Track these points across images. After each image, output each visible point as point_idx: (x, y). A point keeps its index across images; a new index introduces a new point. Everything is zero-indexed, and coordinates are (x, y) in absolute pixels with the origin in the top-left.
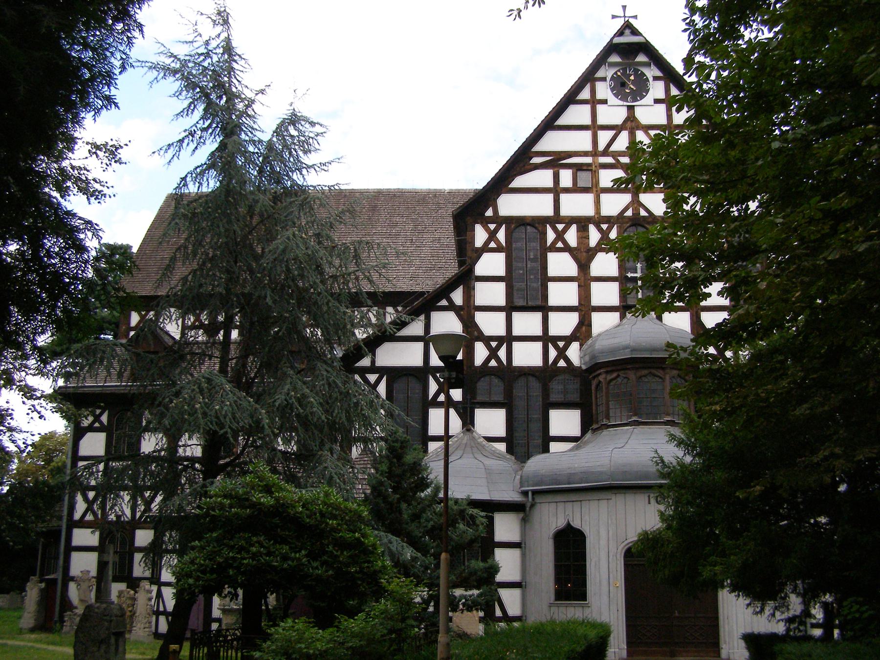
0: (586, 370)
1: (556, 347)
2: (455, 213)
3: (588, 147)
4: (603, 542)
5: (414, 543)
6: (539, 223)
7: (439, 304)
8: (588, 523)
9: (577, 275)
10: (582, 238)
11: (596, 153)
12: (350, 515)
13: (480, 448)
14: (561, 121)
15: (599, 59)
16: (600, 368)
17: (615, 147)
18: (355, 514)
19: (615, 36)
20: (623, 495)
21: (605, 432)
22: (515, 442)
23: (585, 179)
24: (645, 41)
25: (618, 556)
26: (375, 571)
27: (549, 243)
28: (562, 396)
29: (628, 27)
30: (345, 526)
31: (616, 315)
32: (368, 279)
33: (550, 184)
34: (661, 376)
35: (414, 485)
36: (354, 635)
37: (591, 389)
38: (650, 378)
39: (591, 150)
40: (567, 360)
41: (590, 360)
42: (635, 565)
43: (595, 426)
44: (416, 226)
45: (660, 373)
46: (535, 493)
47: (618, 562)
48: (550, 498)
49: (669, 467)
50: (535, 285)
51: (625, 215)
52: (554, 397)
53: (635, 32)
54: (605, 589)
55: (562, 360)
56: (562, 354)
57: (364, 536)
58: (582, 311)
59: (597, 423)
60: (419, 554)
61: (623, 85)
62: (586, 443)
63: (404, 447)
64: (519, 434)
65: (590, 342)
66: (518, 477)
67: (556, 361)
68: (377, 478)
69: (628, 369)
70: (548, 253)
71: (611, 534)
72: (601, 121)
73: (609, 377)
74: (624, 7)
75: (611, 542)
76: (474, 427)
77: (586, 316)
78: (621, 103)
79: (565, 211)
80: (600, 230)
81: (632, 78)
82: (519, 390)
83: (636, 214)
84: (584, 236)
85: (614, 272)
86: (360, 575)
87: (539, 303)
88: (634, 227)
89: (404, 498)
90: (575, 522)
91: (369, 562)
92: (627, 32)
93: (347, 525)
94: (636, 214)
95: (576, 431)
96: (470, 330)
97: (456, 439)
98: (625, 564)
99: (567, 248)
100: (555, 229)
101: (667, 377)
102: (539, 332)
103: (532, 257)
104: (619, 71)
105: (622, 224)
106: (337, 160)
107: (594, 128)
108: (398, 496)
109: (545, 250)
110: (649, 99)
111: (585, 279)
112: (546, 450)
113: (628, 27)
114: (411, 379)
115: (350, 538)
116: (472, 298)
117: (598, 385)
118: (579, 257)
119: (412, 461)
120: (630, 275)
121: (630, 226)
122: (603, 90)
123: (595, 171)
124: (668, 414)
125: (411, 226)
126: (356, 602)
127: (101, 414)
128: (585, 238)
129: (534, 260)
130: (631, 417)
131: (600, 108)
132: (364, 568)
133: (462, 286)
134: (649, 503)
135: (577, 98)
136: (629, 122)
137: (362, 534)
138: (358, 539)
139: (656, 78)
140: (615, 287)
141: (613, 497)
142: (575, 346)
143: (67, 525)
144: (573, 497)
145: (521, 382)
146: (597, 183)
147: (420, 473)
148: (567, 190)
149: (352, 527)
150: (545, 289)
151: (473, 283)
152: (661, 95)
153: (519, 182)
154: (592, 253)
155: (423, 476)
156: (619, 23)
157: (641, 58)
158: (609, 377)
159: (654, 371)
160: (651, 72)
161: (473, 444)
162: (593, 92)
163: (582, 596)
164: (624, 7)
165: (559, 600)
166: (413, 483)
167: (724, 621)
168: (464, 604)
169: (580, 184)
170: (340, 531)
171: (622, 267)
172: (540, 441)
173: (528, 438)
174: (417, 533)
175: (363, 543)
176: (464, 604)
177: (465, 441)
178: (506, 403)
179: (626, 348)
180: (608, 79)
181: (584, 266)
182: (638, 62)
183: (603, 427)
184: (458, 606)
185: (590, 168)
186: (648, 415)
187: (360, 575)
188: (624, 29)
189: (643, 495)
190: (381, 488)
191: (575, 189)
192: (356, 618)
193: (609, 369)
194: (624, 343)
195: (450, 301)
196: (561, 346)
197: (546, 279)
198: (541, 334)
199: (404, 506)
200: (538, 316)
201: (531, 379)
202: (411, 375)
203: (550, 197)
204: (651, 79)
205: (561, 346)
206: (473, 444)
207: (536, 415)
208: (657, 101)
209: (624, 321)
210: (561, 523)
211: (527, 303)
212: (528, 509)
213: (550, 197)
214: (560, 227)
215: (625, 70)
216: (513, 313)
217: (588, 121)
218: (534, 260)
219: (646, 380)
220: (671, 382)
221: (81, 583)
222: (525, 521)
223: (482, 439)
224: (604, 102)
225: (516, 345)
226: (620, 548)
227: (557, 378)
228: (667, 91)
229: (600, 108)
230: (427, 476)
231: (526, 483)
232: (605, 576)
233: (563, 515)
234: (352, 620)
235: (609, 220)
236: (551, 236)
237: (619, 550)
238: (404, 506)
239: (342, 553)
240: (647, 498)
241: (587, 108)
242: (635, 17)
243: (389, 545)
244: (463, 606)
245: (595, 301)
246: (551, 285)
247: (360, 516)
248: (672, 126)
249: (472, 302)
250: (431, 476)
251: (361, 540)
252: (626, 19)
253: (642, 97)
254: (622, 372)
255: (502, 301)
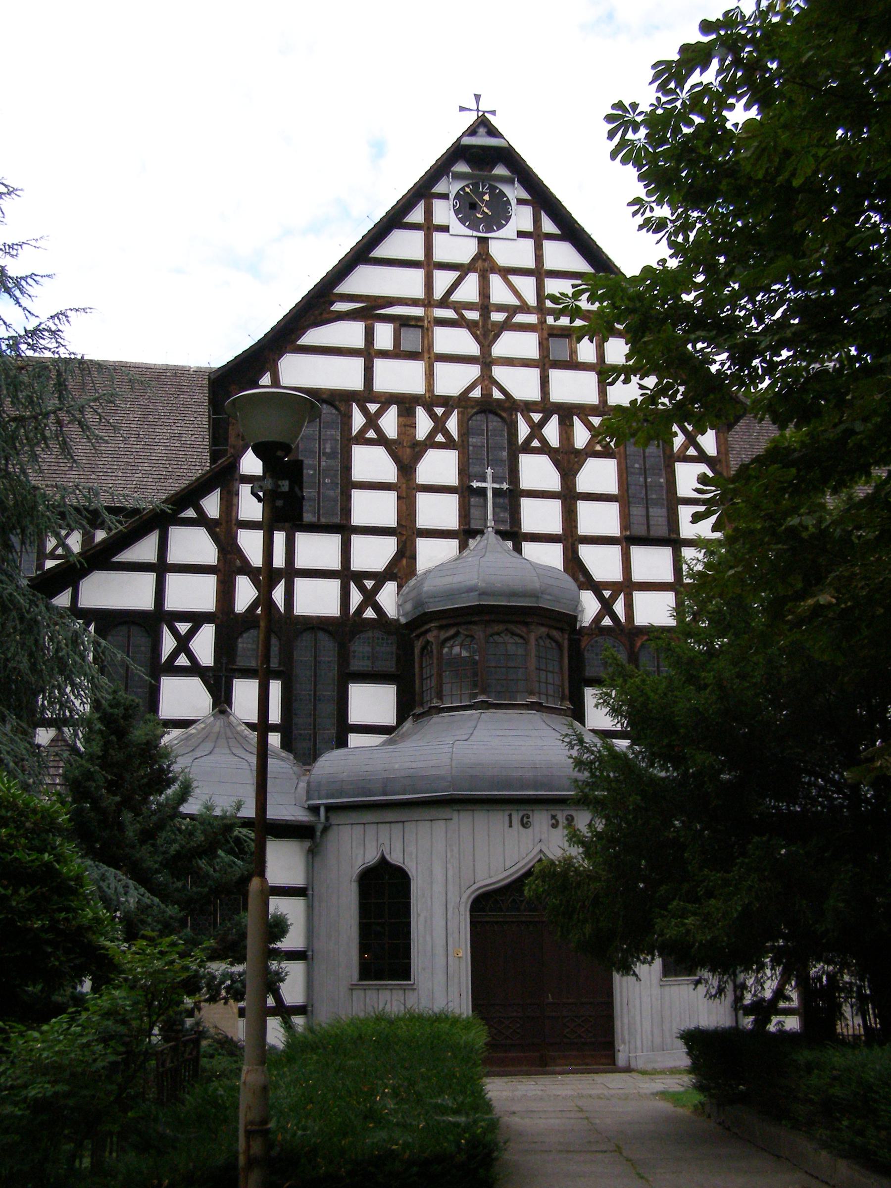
0: (407, 624)
1: (362, 588)
2: (212, 377)
3: (419, 293)
4: (438, 888)
5: (142, 878)
6: (340, 401)
7: (182, 515)
8: (414, 856)
9: (396, 481)
10: (405, 426)
11: (429, 302)
12: (33, 818)
13: (239, 738)
14: (380, 252)
15: (440, 166)
16: (431, 621)
17: (458, 296)
18: (43, 817)
19: (463, 134)
20: (470, 813)
21: (436, 719)
22: (295, 732)
23: (412, 339)
24: (507, 145)
25: (462, 909)
26: (80, 927)
27: (354, 432)
28: (369, 663)
29: (483, 124)
30: (23, 841)
31: (454, 543)
32: (80, 423)
33: (359, 342)
34: (523, 634)
35: (145, 780)
36: (41, 1069)
37: (413, 654)
38: (507, 638)
39: (423, 297)
40: (378, 609)
41: (415, 607)
42: (487, 922)
43: (418, 711)
44: (145, 416)
45: (521, 630)
46: (329, 808)
47: (462, 918)
48: (354, 817)
49: (592, 753)
50: (331, 493)
51: (471, 395)
52: (356, 665)
53: (493, 132)
54: (440, 961)
55: (370, 609)
56: (370, 598)
57: (60, 858)
58: (403, 535)
59: (422, 704)
60: (156, 900)
61: (473, 206)
62: (404, 737)
63: (130, 716)
64: (301, 720)
65: (412, 582)
66: (303, 785)
67: (361, 609)
68: (82, 766)
69: (475, 623)
70: (353, 446)
71: (450, 873)
72: (439, 256)
73: (444, 635)
74: (477, 97)
75: (450, 887)
76: (231, 707)
77: (408, 543)
78: (469, 232)
79: (381, 384)
80: (432, 415)
81: (487, 197)
82: (303, 653)
83: (486, 395)
84: (409, 423)
85: (451, 478)
86: (50, 936)
87: (337, 520)
88: (483, 415)
89: (127, 803)
90: (394, 855)
91: (68, 910)
92: (482, 130)
93: (27, 838)
94: (486, 395)
95: (389, 718)
96: (229, 556)
97: (203, 726)
98: (471, 922)
99: (382, 440)
100: (365, 411)
101: (532, 638)
102: (335, 564)
103: (328, 450)
104: (467, 186)
105: (465, 408)
106: (33, 243)
107: (428, 265)
108: (118, 799)
109: (349, 440)
110: (510, 230)
111: (408, 488)
112: (342, 743)
113: (483, 124)
114: (134, 629)
115: (33, 861)
116: (235, 508)
117: (424, 648)
118: (400, 454)
119: (144, 739)
120: (475, 484)
121: (476, 413)
122: (443, 212)
123: (428, 329)
124: (531, 693)
125: (138, 415)
126: (39, 987)
128: (410, 426)
129: (332, 456)
130: (475, 696)
131: (438, 238)
132: (58, 921)
133: (219, 490)
134: (511, 826)
135: (405, 220)
136: (480, 262)
137: (55, 856)
138: (48, 865)
139: (520, 202)
140: (452, 502)
141: (455, 815)
142: (390, 587)
144: (391, 816)
145: (307, 637)
146: (431, 346)
147: (156, 762)
148: (384, 354)
149: (36, 842)
150: (349, 498)
151: (236, 484)
152: (528, 227)
153: (313, 337)
154: (419, 449)
155: (161, 767)
156: (470, 118)
157: (500, 170)
158: (444, 635)
159: (512, 627)
160: (514, 192)
161: (230, 734)
162: (429, 213)
163: (405, 973)
164: (477, 97)
165: (365, 980)
166: (143, 777)
167: (622, 1009)
168: (228, 989)
169: (405, 346)
170: (13, 848)
171: (464, 471)
172: (333, 731)
173: (315, 728)
174: (151, 863)
175: (58, 873)
176: (228, 989)
177: (216, 729)
178: (282, 671)
179: (471, 590)
180: (452, 197)
181: (407, 469)
182: (495, 175)
183: (433, 711)
184: (219, 993)
185: (420, 324)
186: (499, 694)
187: (50, 936)
188: (478, 126)
189: (501, 813)
190: (89, 783)
191: (397, 353)
192: (45, 1027)
193: (444, 622)
194: (468, 583)
195: (200, 510)
196: (369, 587)
197: (348, 485)
198: (339, 568)
199: (127, 816)
200: (333, 541)
201: (321, 635)
202: (134, 623)
203: (358, 363)
204: (513, 202)
205: (369, 587)
206: (230, 734)
207: (329, 692)
208: (521, 234)
209: (466, 553)
210: (371, 857)
211: (319, 519)
212: (318, 834)
213: (358, 363)
214: (373, 408)
215: (476, 185)
216: (297, 534)
217: (419, 256)
218: (332, 456)
219: (500, 640)
220: (538, 645)
222: (313, 853)
223: (243, 727)
224: (445, 229)
226: (465, 897)
227: (362, 636)
228: (537, 221)
229: (438, 238)
230: (169, 766)
231: (316, 793)
232: (440, 941)
233: (374, 844)
234: (36, 1034)
235: (447, 402)
236: (358, 420)
237: (464, 899)
238: (127, 816)
239: (16, 892)
240: (507, 818)
241: (419, 235)
242: (493, 113)
243: (101, 883)
244: (227, 993)
245: (422, 522)
246: (356, 494)
247: (53, 821)
248: (543, 272)
249: (234, 514)
250: (176, 768)
251: (53, 867)
252: (480, 114)
253: (500, 227)
254: (464, 627)
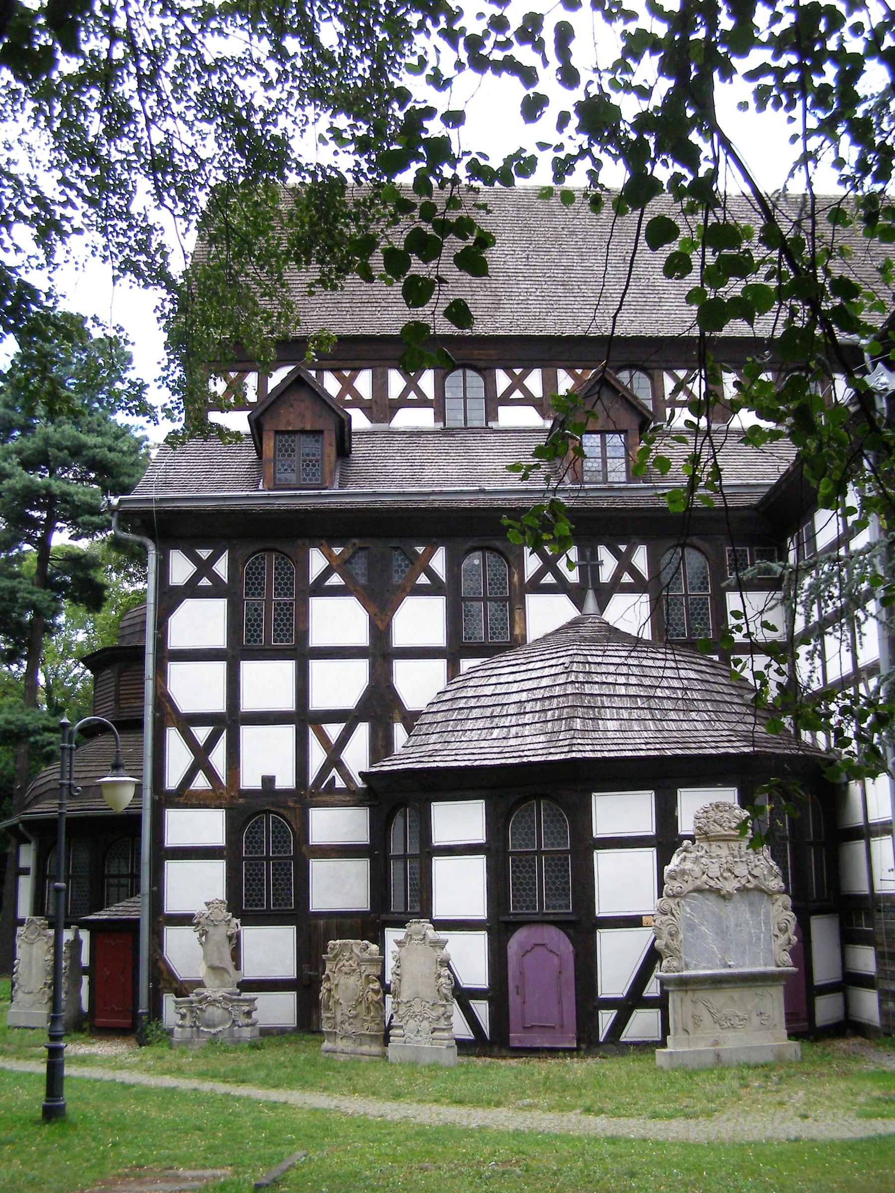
127: (213, 559)
143: (153, 802)
221: (211, 930)
225: (247, 733)
255: (218, 639)
